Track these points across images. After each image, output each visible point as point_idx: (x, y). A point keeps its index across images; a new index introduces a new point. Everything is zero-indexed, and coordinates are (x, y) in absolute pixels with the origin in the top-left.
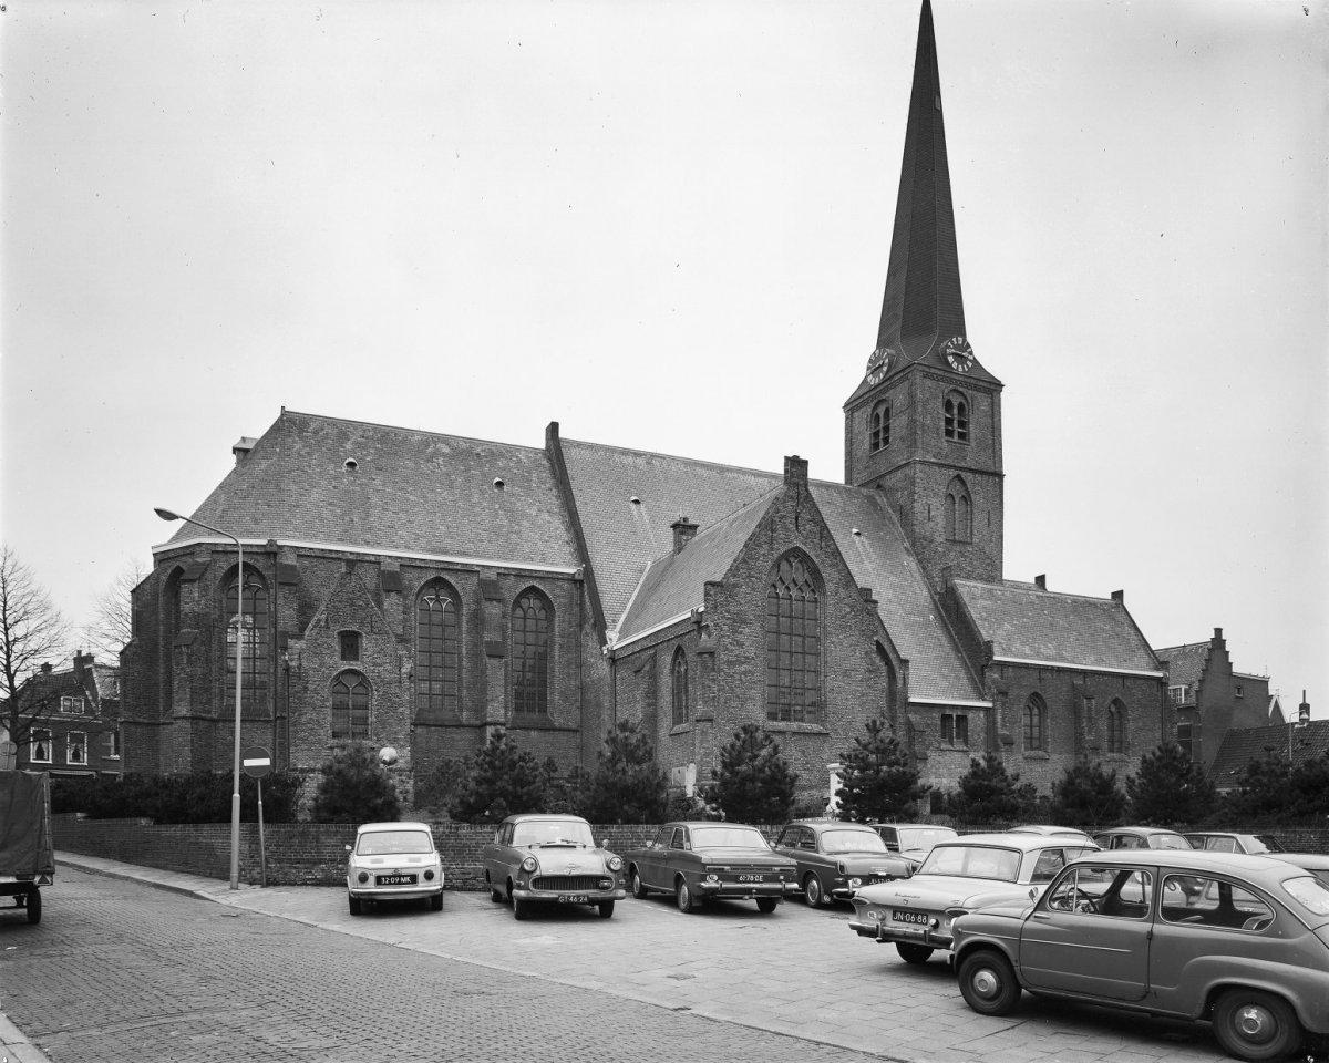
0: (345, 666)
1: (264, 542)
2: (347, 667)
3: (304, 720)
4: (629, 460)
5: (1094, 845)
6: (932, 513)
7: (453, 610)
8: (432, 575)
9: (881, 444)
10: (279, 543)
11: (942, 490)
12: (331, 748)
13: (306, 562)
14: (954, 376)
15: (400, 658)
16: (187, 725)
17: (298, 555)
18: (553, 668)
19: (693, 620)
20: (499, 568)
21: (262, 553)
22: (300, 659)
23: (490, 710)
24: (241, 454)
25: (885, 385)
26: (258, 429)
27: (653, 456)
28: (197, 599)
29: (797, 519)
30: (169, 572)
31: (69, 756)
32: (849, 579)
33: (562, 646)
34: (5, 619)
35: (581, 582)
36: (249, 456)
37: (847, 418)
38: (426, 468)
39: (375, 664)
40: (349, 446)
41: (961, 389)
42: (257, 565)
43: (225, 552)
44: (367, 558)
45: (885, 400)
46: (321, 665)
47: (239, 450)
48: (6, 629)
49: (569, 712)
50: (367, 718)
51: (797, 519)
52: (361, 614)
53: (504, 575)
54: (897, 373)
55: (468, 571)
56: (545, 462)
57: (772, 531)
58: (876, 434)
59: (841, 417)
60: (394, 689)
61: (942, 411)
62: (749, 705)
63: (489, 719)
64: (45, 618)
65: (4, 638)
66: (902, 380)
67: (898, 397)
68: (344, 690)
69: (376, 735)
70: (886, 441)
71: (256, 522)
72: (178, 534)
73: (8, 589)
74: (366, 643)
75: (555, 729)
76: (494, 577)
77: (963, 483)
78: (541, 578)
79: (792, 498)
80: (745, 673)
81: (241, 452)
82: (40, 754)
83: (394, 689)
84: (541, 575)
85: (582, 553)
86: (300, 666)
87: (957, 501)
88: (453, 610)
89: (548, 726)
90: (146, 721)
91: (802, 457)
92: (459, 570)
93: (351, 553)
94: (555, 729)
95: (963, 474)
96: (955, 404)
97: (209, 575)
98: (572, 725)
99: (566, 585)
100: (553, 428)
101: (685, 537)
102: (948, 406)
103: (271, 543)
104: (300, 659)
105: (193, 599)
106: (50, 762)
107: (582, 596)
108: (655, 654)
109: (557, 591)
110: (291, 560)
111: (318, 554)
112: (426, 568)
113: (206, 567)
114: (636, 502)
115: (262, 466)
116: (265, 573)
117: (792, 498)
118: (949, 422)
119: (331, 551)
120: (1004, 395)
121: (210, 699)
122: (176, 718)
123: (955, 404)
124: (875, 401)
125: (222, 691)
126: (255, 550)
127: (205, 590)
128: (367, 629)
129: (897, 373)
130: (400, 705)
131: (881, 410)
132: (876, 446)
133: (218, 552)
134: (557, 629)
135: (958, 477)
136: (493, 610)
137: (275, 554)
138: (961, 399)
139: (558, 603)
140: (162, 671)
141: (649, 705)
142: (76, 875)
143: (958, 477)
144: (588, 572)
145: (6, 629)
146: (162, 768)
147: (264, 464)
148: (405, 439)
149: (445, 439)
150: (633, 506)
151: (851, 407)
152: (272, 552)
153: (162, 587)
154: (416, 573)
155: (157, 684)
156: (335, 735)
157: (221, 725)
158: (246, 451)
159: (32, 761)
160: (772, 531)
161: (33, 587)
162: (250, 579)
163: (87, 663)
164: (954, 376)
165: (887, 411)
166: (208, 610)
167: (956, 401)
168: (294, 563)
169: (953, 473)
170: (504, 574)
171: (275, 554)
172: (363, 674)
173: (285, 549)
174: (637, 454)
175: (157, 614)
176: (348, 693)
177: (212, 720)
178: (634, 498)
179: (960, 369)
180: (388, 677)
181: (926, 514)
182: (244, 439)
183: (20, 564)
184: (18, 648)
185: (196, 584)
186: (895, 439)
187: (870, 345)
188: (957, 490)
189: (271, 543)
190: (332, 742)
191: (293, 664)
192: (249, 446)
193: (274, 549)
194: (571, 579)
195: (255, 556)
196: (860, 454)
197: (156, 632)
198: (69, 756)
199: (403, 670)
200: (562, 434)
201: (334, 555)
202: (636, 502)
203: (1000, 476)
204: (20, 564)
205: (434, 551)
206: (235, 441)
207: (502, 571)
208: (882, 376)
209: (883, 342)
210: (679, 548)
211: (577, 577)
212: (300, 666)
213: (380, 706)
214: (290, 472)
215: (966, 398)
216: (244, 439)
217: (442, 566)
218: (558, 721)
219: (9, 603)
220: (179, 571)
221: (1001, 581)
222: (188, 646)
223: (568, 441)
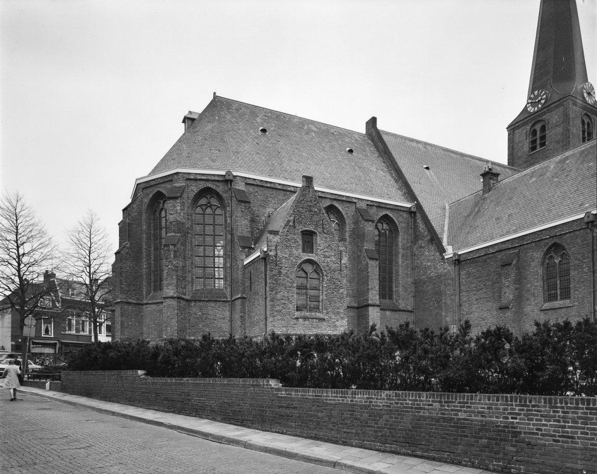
0: (306, 257)
1: (223, 173)
2: (307, 258)
3: (279, 296)
4: (414, 144)
7: (338, 229)
9: (538, 147)
10: (235, 174)
12: (297, 319)
13: (251, 189)
15: (341, 251)
16: (174, 303)
17: (246, 183)
18: (397, 272)
19: (586, 220)
20: (368, 200)
21: (222, 181)
22: (276, 250)
23: (370, 296)
24: (190, 122)
25: (542, 111)
26: (199, 106)
27: (426, 144)
28: (179, 211)
30: (151, 196)
31: (43, 332)
33: (403, 255)
34: (17, 240)
35: (415, 213)
36: (195, 122)
37: (509, 135)
38: (306, 138)
39: (325, 257)
40: (259, 120)
41: (589, 114)
42: (218, 190)
43: (196, 180)
44: (289, 189)
45: (542, 120)
46: (290, 255)
47: (189, 119)
48: (18, 247)
49: (407, 299)
50: (319, 297)
52: (316, 218)
53: (370, 205)
54: (555, 103)
55: (349, 201)
56: (370, 142)
58: (534, 142)
59: (506, 134)
60: (337, 275)
63: (370, 302)
64: (42, 241)
65: (16, 252)
66: (557, 107)
67: (554, 118)
68: (304, 275)
69: (326, 309)
70: (543, 144)
71: (213, 161)
72: (156, 167)
73: (19, 221)
74: (320, 241)
75: (400, 310)
76: (365, 207)
78: (391, 209)
82: (47, 331)
83: (337, 275)
84: (391, 207)
85: (410, 195)
86: (276, 255)
88: (338, 229)
89: (395, 308)
90: (134, 302)
92: (343, 201)
93: (280, 184)
94: (400, 310)
96: (586, 122)
97: (185, 195)
98: (410, 308)
99: (405, 215)
100: (372, 122)
101: (492, 182)
102: (583, 122)
103: (229, 173)
104: (276, 250)
105: (174, 212)
106: (52, 336)
107: (415, 222)
108: (518, 254)
109: (401, 219)
110: (241, 186)
112: (325, 198)
113: (182, 190)
114: (427, 168)
115: (208, 127)
116: (224, 195)
119: (266, 182)
121: (186, 285)
122: (165, 298)
123: (586, 122)
124: (534, 121)
125: (192, 279)
126: (217, 178)
127: (183, 204)
128: (320, 230)
129: (555, 103)
130: (341, 287)
131: (538, 127)
132: (533, 148)
133: (190, 179)
134: (400, 244)
136: (369, 228)
137: (231, 181)
139: (401, 226)
140: (145, 266)
141: (516, 289)
142: (71, 407)
144: (419, 206)
145: (18, 247)
146: (145, 335)
147: (210, 126)
148: (290, 120)
149: (313, 122)
150: (426, 171)
151: (512, 128)
152: (228, 181)
153: (145, 207)
155: (141, 276)
156: (298, 309)
157: (193, 304)
158: (193, 120)
159: (43, 336)
161: (35, 220)
162: (211, 200)
163: (51, 277)
165: (543, 129)
166: (184, 220)
167: (587, 120)
168: (244, 189)
170: (371, 205)
171: (231, 181)
172: (316, 263)
174: (418, 142)
175: (141, 226)
176: (307, 278)
177: (187, 300)
178: (425, 166)
180: (334, 266)
183: (27, 205)
184: (25, 259)
185: (179, 201)
186: (551, 143)
189: (229, 173)
190: (297, 314)
191: (272, 253)
193: (231, 178)
194: (409, 211)
195: (216, 183)
196: (519, 154)
197: (140, 239)
198: (43, 332)
199: (343, 262)
200: (380, 126)
201: (269, 185)
202: (427, 168)
204: (27, 205)
205: (327, 187)
206: (186, 113)
207: (369, 203)
208: (540, 106)
210: (487, 188)
211: (413, 210)
212: (276, 255)
213: (328, 288)
214: (228, 131)
215: (591, 120)
216: (190, 112)
217: (334, 197)
218: (402, 305)
219: (20, 231)
220: (159, 196)
222: (174, 245)
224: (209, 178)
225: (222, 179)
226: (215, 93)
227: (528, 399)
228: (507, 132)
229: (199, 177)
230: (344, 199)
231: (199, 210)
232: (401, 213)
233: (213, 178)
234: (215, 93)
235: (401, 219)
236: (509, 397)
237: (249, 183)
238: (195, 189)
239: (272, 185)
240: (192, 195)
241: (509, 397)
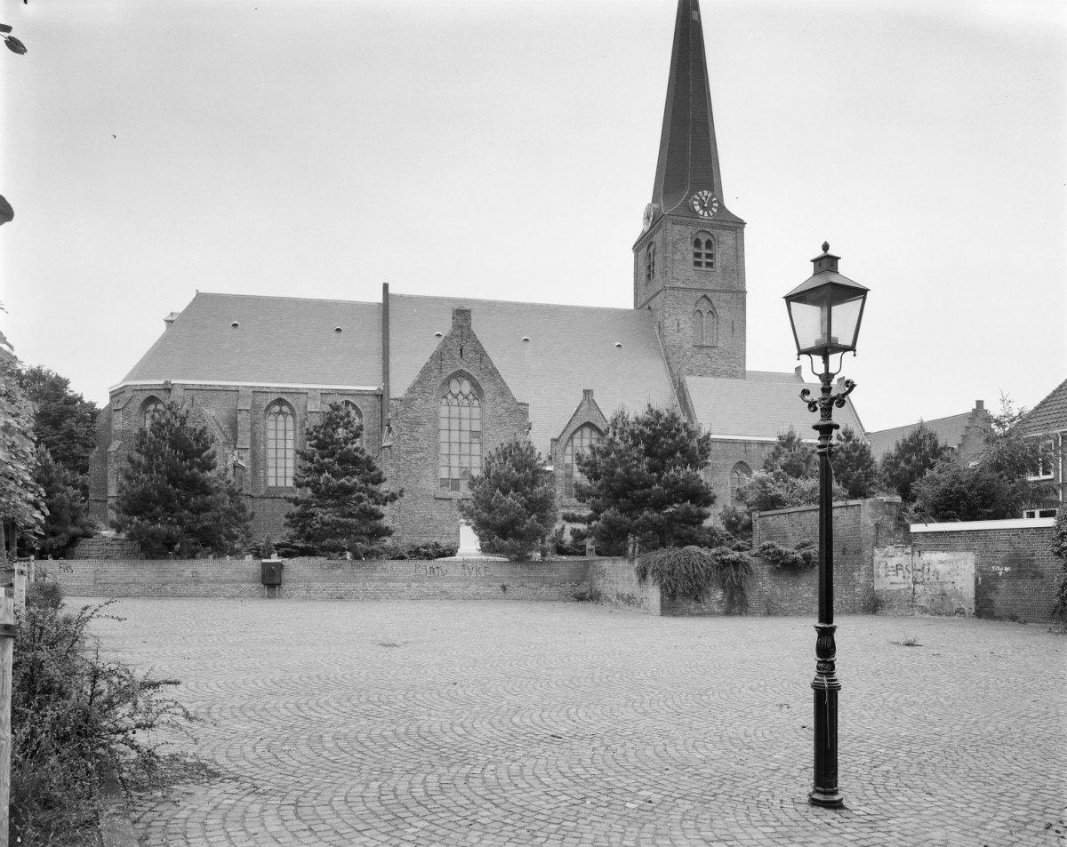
5: (107, 600)
6: (681, 326)
8: (275, 397)
10: (173, 382)
11: (691, 308)
14: (700, 221)
20: (322, 389)
26: (180, 308)
29: (461, 350)
32: (504, 391)
35: (381, 396)
41: (707, 230)
51: (461, 350)
57: (442, 361)
59: (632, 255)
61: (691, 248)
62: (423, 481)
77: (709, 300)
79: (457, 336)
80: (420, 459)
81: (169, 322)
87: (705, 315)
91: (745, 221)
95: (709, 295)
99: (371, 399)
102: (697, 243)
109: (365, 404)
111: (198, 387)
117: (457, 336)
118: (698, 255)
120: (746, 230)
123: (703, 242)
127: (128, 414)
133: (137, 390)
135: (705, 296)
137: (170, 390)
138: (708, 237)
143: (705, 296)
151: (637, 248)
154: (264, 396)
158: (172, 322)
160: (442, 361)
164: (700, 221)
167: (704, 239)
169: (700, 294)
171: (170, 390)
173: (176, 386)
179: (706, 214)
181: (675, 327)
182: (172, 314)
187: (647, 197)
188: (704, 306)
189: (166, 383)
192: (174, 318)
200: (391, 291)
203: (744, 292)
206: (166, 315)
209: (655, 199)
216: (172, 314)
221: (744, 375)
223: (395, 296)
224: (152, 387)
225: (162, 387)
226: (386, 286)
227: (56, 447)
228: (734, 202)
229: (143, 388)
230: (293, 391)
231: (272, 417)
232: (366, 397)
233: (155, 387)
234: (386, 286)
235: (365, 404)
236: (1041, 473)
237: (186, 388)
238: (142, 397)
239: (213, 388)
240: (138, 404)
241: (1041, 473)
